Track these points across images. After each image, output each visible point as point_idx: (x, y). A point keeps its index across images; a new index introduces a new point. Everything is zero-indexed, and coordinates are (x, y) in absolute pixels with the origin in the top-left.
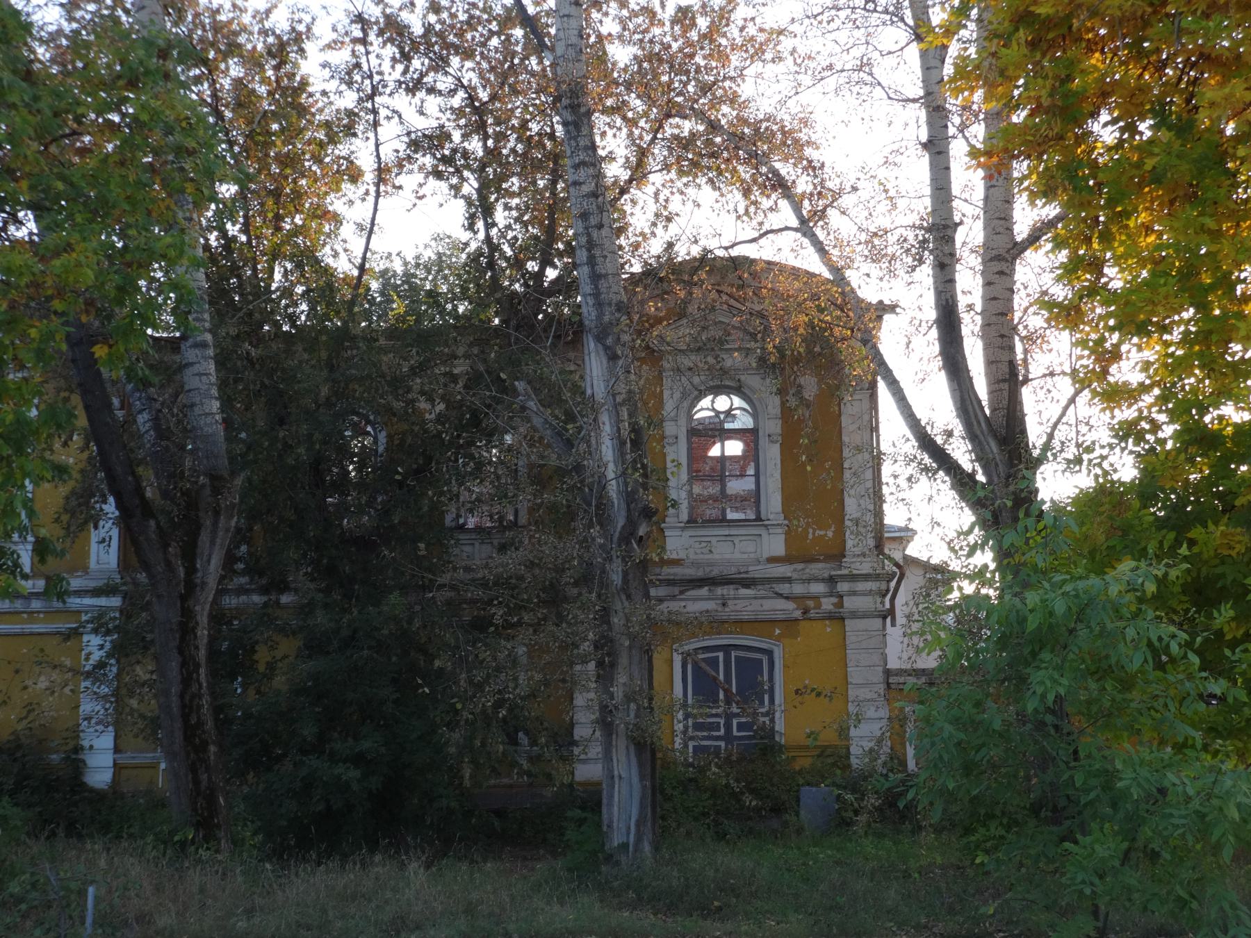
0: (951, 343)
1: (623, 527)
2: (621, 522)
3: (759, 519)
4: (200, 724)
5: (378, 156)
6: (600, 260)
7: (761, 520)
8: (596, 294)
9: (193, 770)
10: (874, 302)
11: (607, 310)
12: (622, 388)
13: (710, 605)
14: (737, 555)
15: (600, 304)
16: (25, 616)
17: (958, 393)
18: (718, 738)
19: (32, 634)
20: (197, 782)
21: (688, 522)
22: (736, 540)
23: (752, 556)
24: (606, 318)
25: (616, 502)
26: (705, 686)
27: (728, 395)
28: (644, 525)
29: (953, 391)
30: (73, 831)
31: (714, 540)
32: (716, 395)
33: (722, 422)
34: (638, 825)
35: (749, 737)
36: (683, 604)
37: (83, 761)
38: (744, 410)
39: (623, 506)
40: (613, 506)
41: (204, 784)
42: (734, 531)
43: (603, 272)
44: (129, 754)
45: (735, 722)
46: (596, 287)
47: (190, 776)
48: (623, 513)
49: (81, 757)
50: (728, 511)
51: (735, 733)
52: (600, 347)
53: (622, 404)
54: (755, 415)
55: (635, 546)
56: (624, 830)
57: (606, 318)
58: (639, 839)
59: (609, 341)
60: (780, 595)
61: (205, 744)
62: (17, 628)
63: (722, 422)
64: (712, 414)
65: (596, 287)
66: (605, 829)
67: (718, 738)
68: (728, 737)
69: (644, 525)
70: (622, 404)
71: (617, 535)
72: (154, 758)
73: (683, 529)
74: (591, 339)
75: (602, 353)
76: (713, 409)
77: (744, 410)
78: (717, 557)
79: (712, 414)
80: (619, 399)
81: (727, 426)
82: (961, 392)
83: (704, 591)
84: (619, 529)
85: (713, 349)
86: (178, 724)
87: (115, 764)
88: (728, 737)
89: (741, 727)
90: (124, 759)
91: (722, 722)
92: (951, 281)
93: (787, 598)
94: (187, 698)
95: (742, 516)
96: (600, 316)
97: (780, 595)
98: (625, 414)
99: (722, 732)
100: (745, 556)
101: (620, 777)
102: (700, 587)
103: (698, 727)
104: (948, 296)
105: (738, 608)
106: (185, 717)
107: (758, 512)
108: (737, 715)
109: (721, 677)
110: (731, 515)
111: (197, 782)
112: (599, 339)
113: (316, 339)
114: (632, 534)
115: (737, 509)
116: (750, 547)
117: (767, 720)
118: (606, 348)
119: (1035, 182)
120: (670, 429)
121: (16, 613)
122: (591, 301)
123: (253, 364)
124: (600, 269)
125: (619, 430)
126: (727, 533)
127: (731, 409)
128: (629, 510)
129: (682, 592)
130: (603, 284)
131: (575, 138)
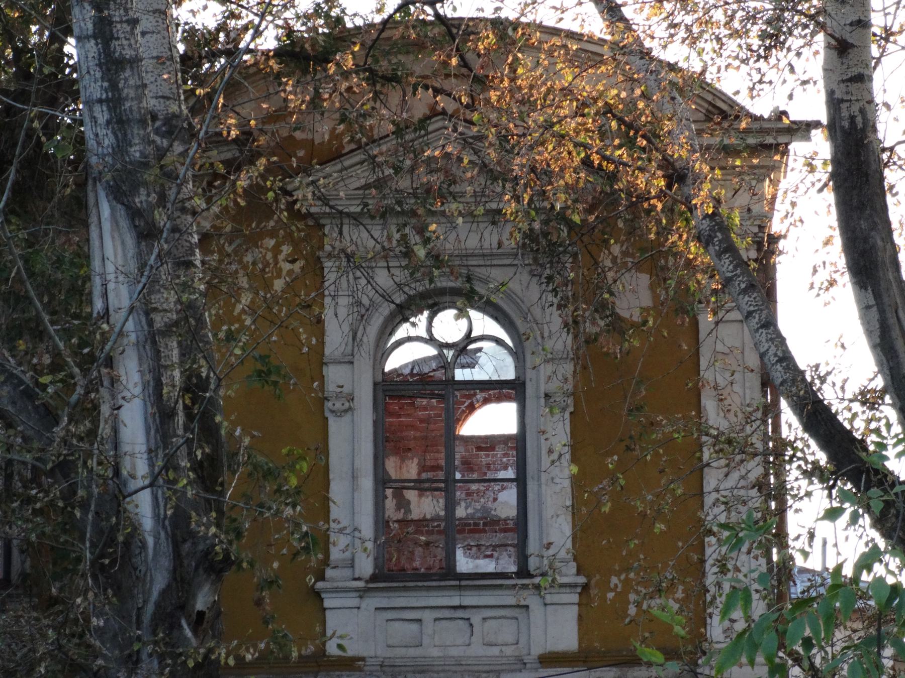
0: (861, 207)
1: (164, 593)
2: (159, 581)
3: (523, 572)
6: (121, 29)
7: (530, 576)
8: (114, 101)
12: (167, 300)
14: (477, 650)
17: (874, 313)
21: (374, 578)
22: (476, 618)
23: (509, 651)
24: (135, 152)
25: (150, 541)
28: (206, 588)
29: (865, 310)
31: (427, 616)
32: (435, 310)
33: (447, 367)
38: (498, 341)
39: (166, 546)
40: (144, 546)
42: (470, 599)
43: (128, 53)
46: (114, 86)
48: (166, 562)
50: (459, 554)
52: (121, 211)
53: (167, 331)
54: (518, 354)
55: (188, 633)
57: (135, 152)
59: (141, 199)
63: (447, 367)
64: (431, 351)
65: (114, 86)
69: (206, 588)
70: (167, 331)
71: (150, 608)
73: (362, 593)
74: (102, 194)
75: (124, 223)
76: (431, 340)
77: (498, 341)
78: (435, 652)
79: (431, 351)
80: (159, 321)
81: (461, 375)
82: (882, 312)
84: (155, 594)
85: (414, 213)
92: (862, 79)
95: (488, 566)
96: (122, 146)
98: (172, 351)
100: (495, 651)
104: (855, 109)
107: (523, 558)
110: (464, 563)
112: (118, 194)
114: (183, 607)
115: (479, 551)
116: (505, 631)
118: (134, 214)
119: (109, 9)
120: (335, 376)
122: (102, 115)
123: (681, 91)
124: (122, 48)
125: (159, 385)
126: (456, 601)
127: (469, 338)
128: (177, 556)
130: (128, 80)
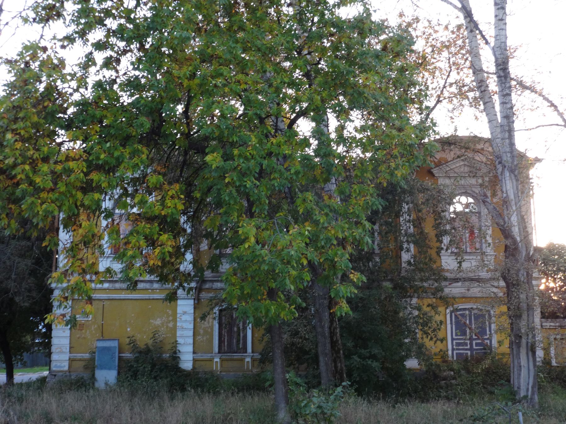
4: (337, 341)
5: (532, 89)
9: (335, 361)
10: (534, 157)
11: (516, 159)
13: (463, 290)
15: (513, 156)
16: (150, 291)
18: (466, 350)
19: (153, 299)
20: (336, 367)
26: (461, 327)
27: (467, 197)
30: (183, 389)
32: (461, 196)
34: (532, 388)
35: (481, 349)
36: (450, 289)
37: (179, 357)
41: (339, 368)
44: (199, 354)
45: (474, 342)
47: (333, 364)
49: (177, 355)
51: (474, 347)
56: (525, 390)
58: (533, 394)
60: (494, 286)
61: (339, 350)
62: (147, 296)
66: (516, 389)
67: (466, 350)
68: (471, 349)
72: (211, 356)
73: (449, 256)
83: (460, 284)
86: (328, 341)
87: (193, 359)
88: (471, 349)
89: (477, 344)
90: (199, 356)
91: (468, 342)
93: (496, 287)
94: (332, 328)
97: (494, 286)
99: (469, 347)
101: (524, 366)
102: (458, 282)
103: (458, 344)
105: (474, 291)
106: (331, 338)
108: (475, 339)
109: (468, 322)
111: (336, 367)
113: (193, 163)
117: (488, 341)
121: (146, 289)
129: (450, 284)
131: (504, 83)
